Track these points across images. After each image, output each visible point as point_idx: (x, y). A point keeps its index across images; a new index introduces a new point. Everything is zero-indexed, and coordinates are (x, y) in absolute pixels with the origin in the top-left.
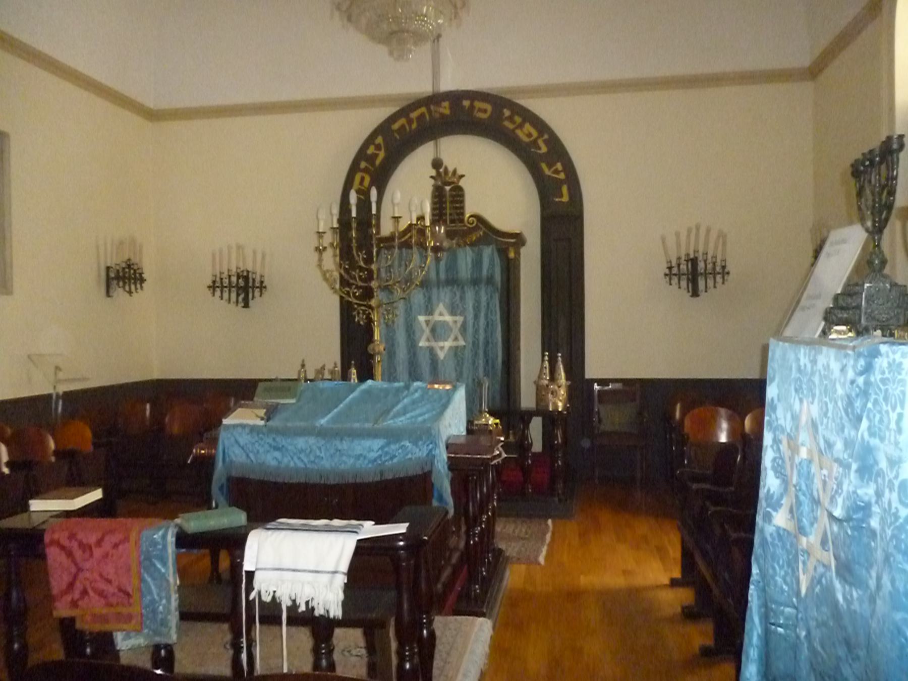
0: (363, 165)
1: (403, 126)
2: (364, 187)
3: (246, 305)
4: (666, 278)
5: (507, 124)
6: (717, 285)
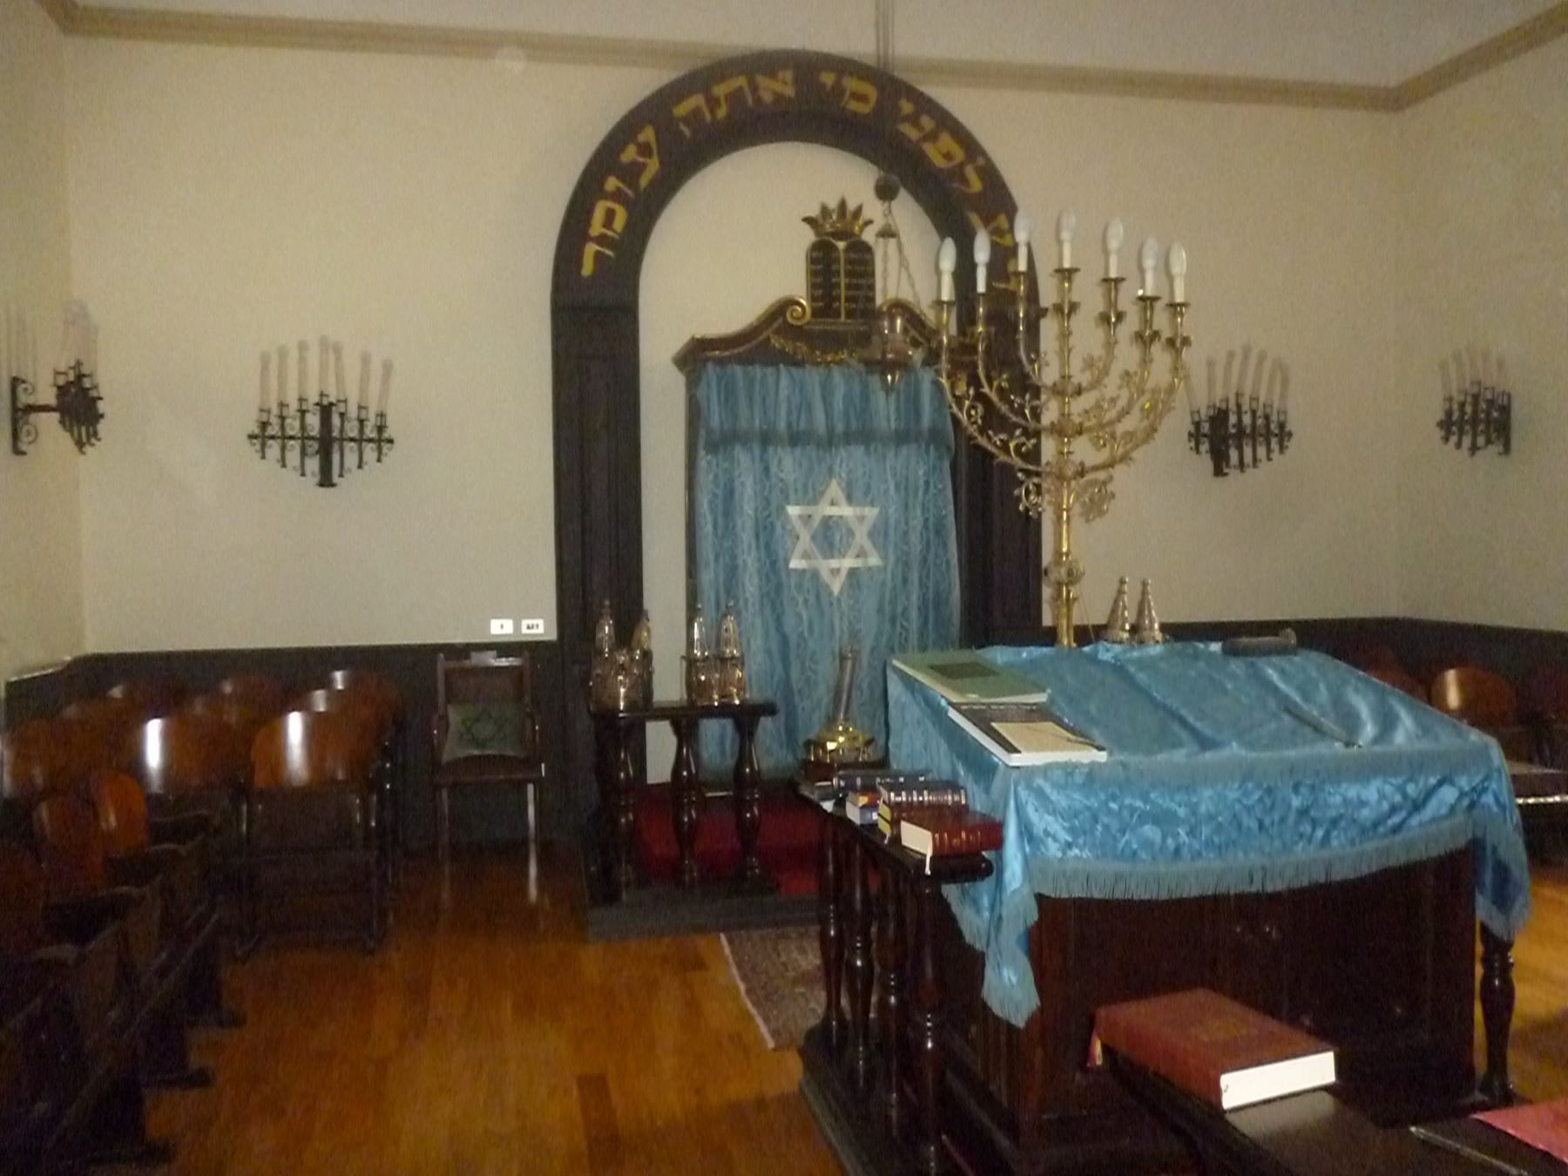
0: (612, 183)
1: (696, 112)
2: (614, 231)
3: (326, 481)
4: (1190, 441)
5: (908, 130)
6: (1272, 456)
